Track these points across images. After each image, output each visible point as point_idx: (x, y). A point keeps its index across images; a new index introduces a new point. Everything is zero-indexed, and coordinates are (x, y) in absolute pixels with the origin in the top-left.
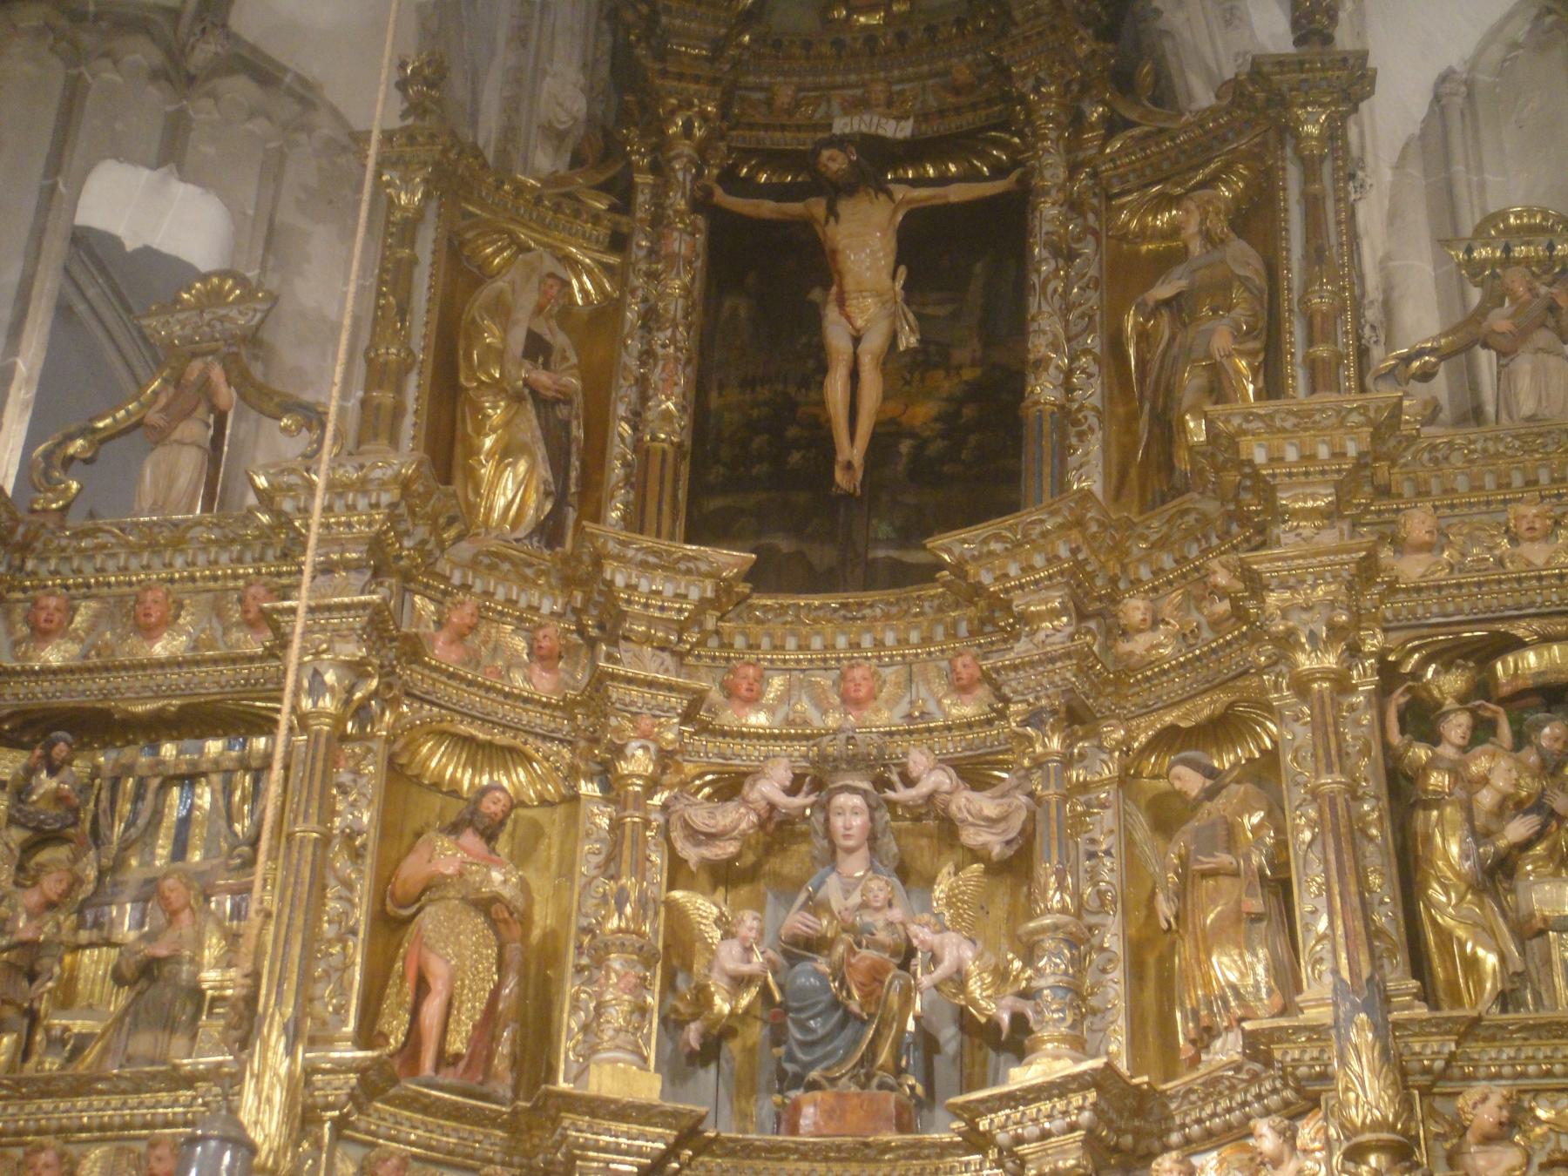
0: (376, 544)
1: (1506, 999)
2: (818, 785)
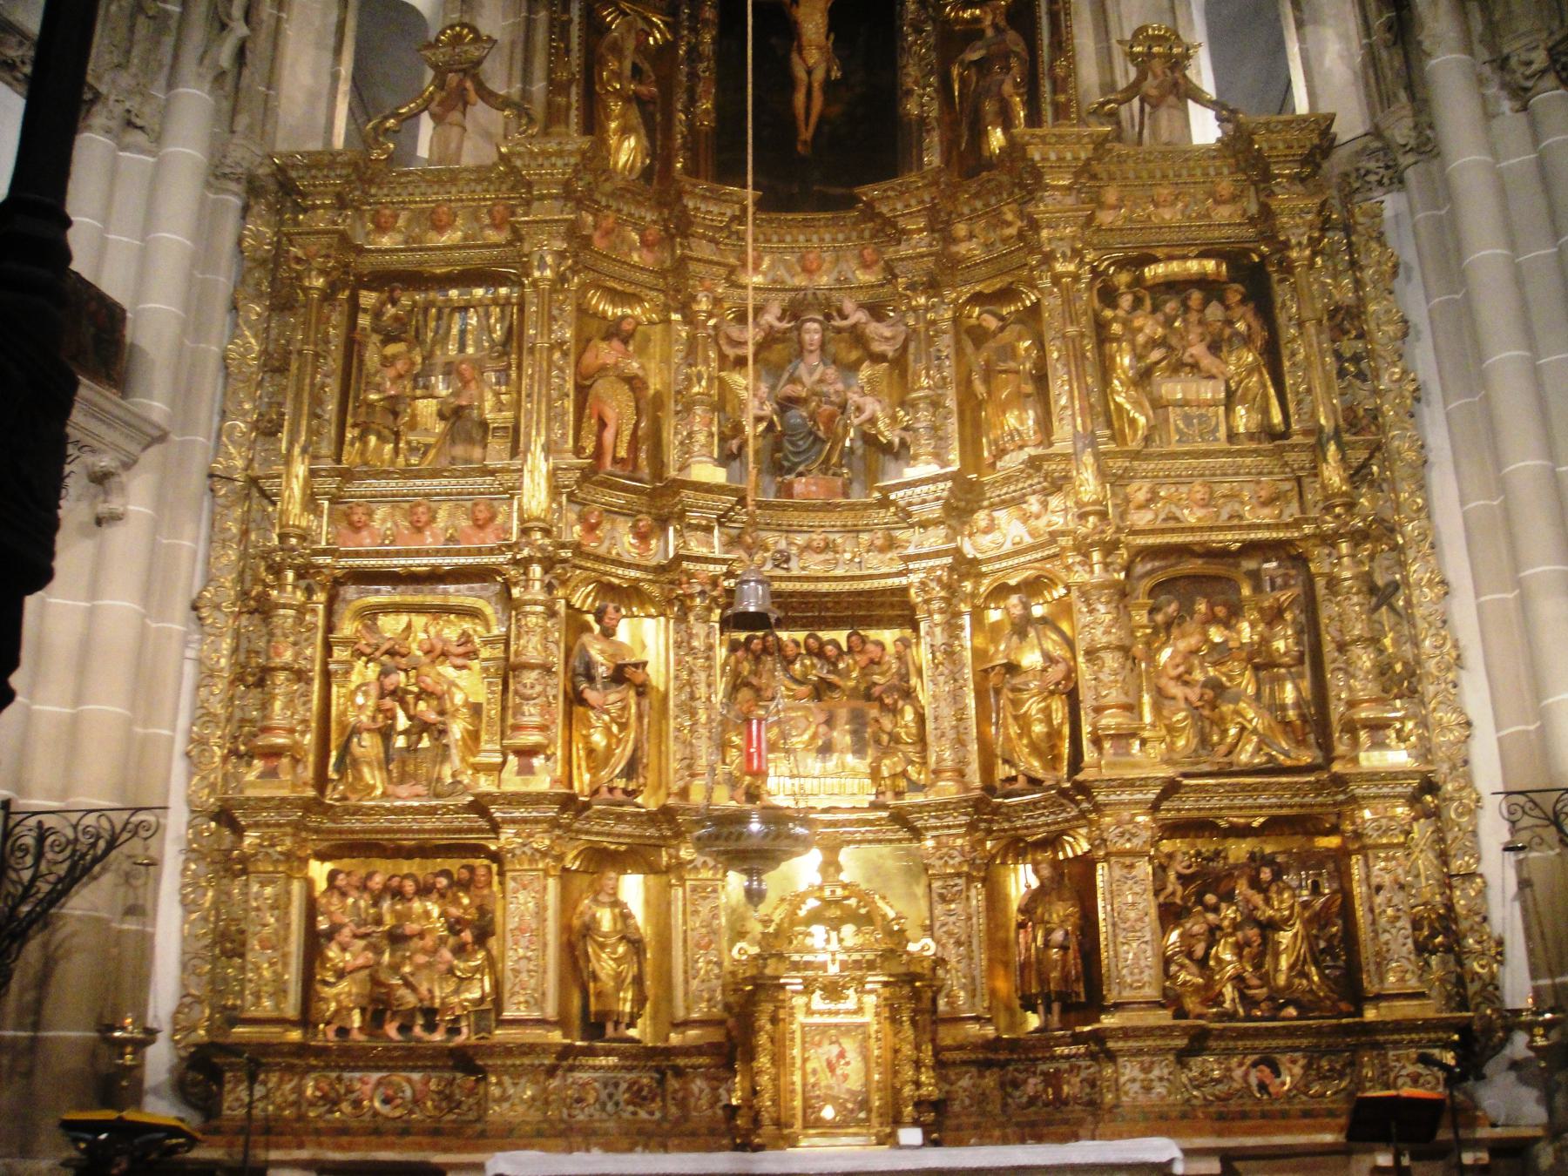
0: (567, 185)
1: (1147, 439)
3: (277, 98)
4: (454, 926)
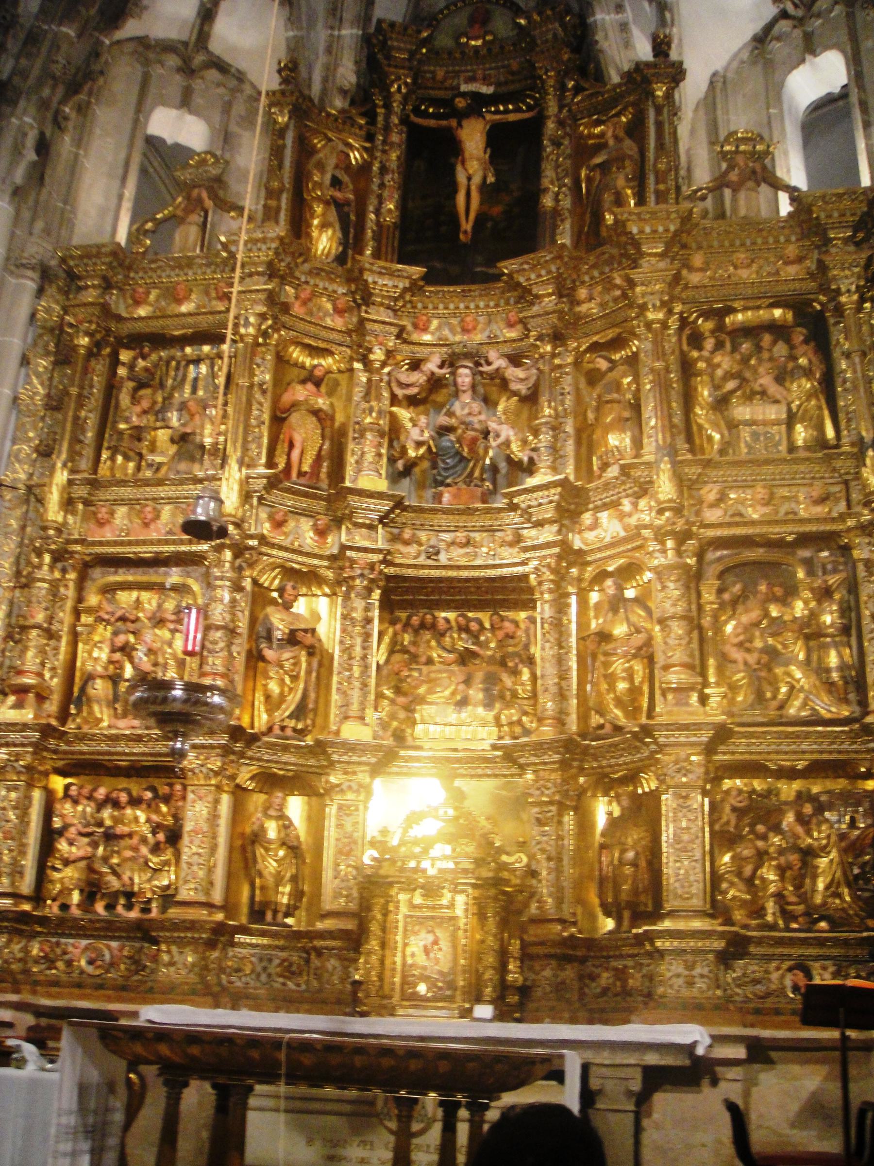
0: (270, 264)
1: (722, 452)
2: (452, 365)
3: (74, 212)
4: (156, 829)
